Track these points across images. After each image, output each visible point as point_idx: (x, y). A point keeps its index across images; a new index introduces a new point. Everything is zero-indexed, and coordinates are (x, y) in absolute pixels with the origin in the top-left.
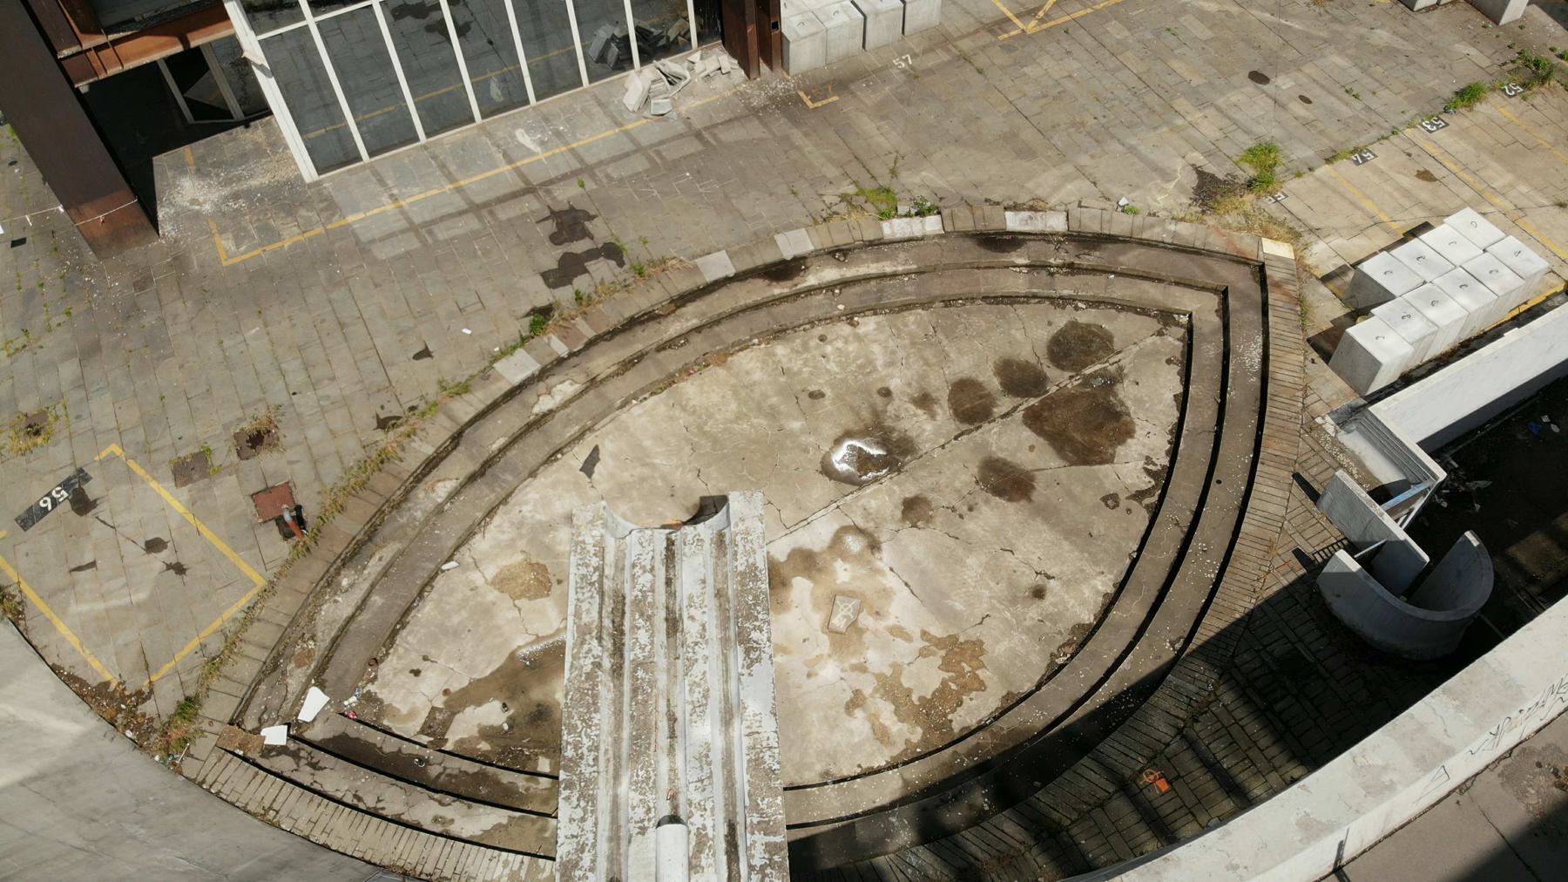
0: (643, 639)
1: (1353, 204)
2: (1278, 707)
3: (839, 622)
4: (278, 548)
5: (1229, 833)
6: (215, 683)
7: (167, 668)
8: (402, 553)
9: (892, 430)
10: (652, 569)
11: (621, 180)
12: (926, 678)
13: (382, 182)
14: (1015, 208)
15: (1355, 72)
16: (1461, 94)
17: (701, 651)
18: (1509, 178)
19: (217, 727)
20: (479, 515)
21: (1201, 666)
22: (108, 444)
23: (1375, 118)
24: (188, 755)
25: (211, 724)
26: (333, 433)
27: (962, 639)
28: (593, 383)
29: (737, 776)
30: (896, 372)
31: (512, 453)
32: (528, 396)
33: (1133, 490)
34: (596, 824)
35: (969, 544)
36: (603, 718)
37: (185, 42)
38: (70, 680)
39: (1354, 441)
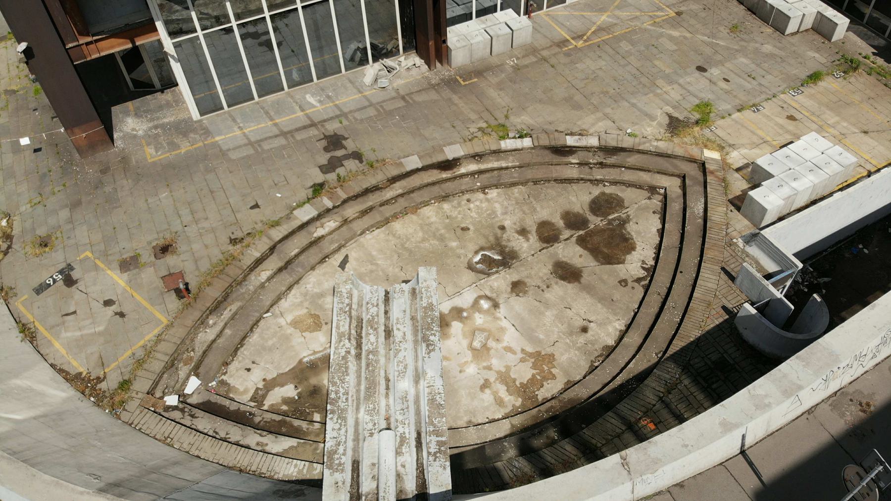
0: (372, 340)
1: (752, 132)
2: (714, 386)
3: (477, 344)
4: (173, 303)
6: (140, 373)
8: (241, 308)
9: (506, 247)
10: (377, 305)
11: (362, 120)
12: (524, 373)
13: (234, 120)
14: (572, 134)
15: (753, 66)
17: (403, 346)
18: (837, 119)
19: (140, 395)
20: (284, 289)
21: (671, 365)
22: (84, 251)
23: (764, 89)
24: (124, 409)
25: (137, 394)
26: (206, 246)
28: (345, 222)
29: (422, 409)
30: (508, 217)
32: (311, 228)
34: (346, 432)
35: (547, 305)
36: (351, 379)
37: (133, 42)
38: (61, 371)
39: (753, 250)
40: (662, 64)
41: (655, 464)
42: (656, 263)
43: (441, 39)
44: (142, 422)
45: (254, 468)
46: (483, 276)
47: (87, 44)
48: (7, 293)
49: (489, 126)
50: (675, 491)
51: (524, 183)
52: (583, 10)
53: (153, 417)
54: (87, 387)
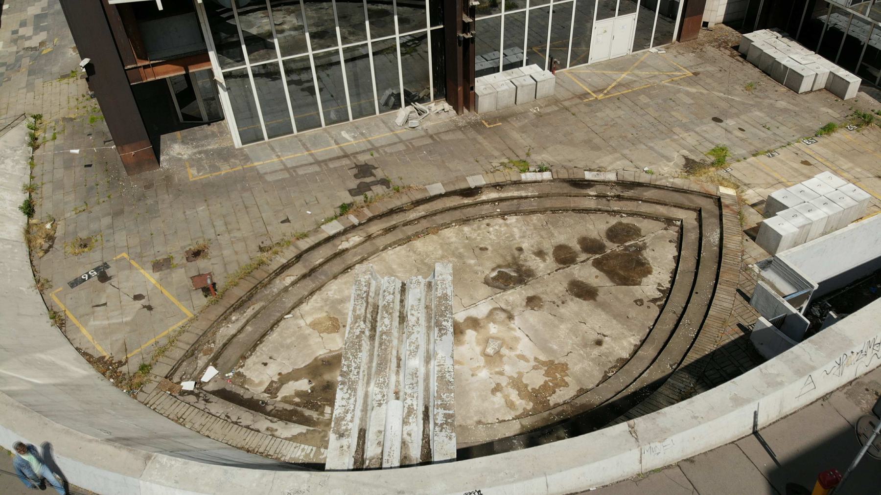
0: (385, 323)
1: (767, 174)
3: (490, 351)
4: (201, 300)
5: (693, 402)
6: (161, 359)
7: (136, 352)
8: (264, 308)
9: (523, 266)
10: (394, 293)
11: (391, 154)
12: (536, 380)
13: (273, 149)
14: (590, 170)
15: (768, 119)
16: (824, 129)
17: (416, 329)
18: (850, 165)
19: (158, 379)
20: (306, 293)
21: (685, 376)
22: (121, 252)
23: (778, 138)
24: (141, 391)
25: (155, 377)
26: (236, 253)
27: (556, 362)
28: (369, 237)
29: (431, 385)
30: (526, 240)
31: (326, 267)
32: (336, 241)
33: (651, 298)
34: (355, 401)
35: (562, 319)
36: (364, 356)
37: (187, 70)
38: (85, 354)
39: (769, 274)
40: (679, 115)
41: (663, 434)
42: (672, 286)
43: (470, 87)
44: (157, 403)
45: (261, 450)
46: (499, 291)
47: (145, 67)
48: (43, 285)
49: (511, 162)
50: (685, 466)
51: (543, 211)
52: (604, 70)
53: (168, 400)
54: (109, 369)
